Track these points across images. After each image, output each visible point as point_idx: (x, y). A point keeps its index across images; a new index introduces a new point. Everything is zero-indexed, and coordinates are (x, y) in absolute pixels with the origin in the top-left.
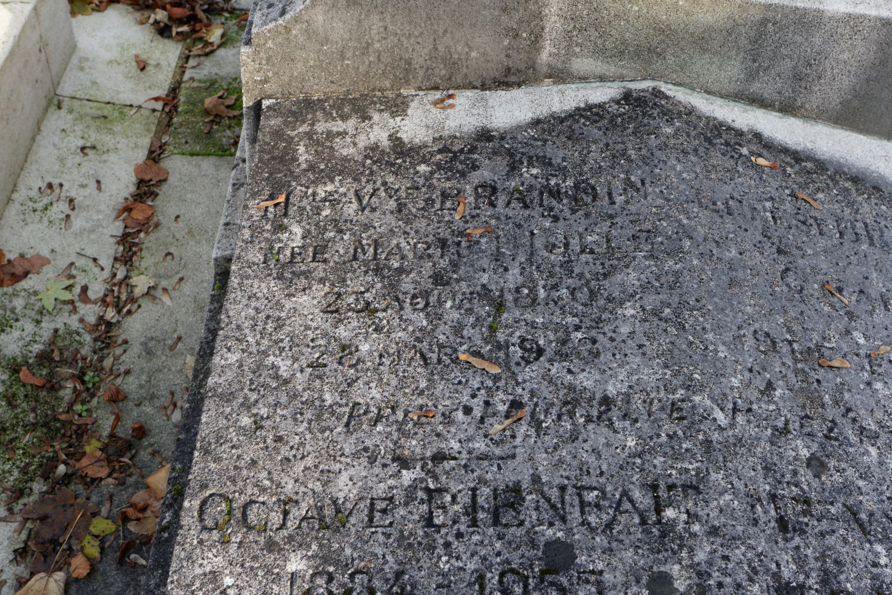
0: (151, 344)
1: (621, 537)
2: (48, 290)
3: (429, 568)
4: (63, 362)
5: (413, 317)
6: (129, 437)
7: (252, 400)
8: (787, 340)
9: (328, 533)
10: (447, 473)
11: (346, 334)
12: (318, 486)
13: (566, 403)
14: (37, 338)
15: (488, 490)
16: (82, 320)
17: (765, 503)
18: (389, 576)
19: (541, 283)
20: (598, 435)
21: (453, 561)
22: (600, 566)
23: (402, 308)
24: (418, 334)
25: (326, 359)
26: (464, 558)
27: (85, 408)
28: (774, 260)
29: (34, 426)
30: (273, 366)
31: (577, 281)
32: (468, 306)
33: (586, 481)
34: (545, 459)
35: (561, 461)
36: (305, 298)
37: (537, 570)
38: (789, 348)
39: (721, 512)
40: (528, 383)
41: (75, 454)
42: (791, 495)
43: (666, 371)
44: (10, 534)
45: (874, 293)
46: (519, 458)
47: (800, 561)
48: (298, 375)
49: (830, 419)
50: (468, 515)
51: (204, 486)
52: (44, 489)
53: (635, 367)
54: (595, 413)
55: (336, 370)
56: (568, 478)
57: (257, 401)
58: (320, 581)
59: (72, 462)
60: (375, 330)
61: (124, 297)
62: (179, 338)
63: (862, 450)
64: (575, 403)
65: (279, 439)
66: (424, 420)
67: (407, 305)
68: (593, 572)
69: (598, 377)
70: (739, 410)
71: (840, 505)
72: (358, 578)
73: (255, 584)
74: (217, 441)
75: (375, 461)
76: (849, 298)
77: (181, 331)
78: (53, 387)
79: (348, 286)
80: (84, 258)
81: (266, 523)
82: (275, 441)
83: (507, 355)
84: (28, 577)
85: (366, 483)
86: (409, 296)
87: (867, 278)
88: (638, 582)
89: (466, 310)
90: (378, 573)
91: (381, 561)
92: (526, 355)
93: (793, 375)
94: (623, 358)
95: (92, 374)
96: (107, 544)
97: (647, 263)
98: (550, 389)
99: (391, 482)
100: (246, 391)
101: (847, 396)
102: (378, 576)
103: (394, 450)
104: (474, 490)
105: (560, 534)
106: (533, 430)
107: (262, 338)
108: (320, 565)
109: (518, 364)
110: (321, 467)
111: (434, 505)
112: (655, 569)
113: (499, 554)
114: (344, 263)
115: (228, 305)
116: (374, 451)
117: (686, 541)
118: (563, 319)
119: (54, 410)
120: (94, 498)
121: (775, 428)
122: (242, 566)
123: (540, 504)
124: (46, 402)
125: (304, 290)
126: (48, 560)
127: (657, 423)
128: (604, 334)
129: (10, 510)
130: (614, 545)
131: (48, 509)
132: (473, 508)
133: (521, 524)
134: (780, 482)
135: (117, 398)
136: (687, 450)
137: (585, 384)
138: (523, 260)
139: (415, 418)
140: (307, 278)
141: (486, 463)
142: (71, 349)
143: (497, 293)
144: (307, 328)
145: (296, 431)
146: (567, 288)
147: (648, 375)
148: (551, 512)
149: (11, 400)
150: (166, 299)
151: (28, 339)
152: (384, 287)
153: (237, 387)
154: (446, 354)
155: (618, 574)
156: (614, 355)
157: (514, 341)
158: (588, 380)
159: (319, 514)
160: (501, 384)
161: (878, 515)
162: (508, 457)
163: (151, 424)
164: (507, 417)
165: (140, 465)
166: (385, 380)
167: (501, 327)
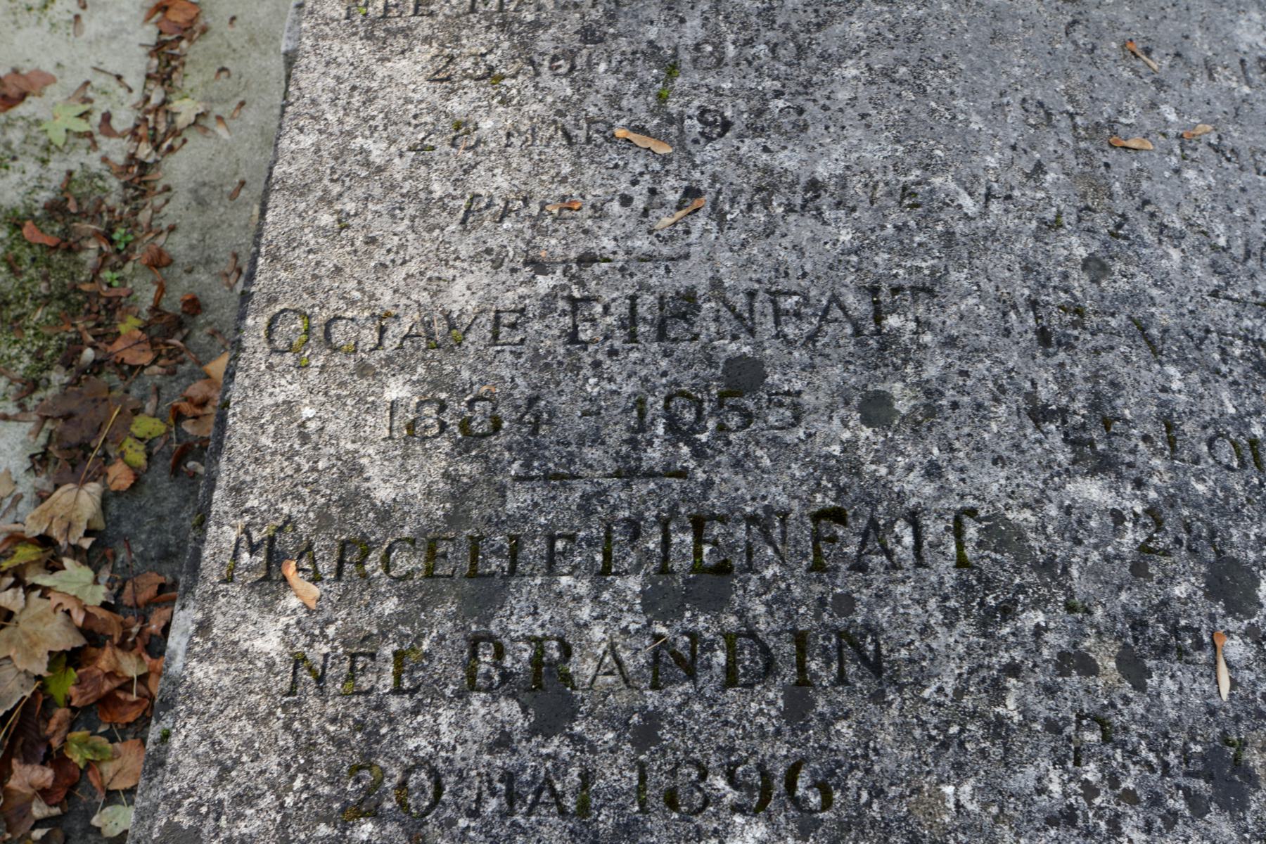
1: (827, 351)
2: (55, 118)
3: (572, 392)
4: (82, 215)
5: (553, 84)
6: (179, 313)
7: (335, 193)
8: (1067, 112)
9: (438, 354)
10: (598, 278)
11: (461, 108)
12: (425, 298)
13: (759, 190)
14: (45, 184)
15: (652, 298)
16: (105, 160)
17: (1021, 310)
18: (519, 402)
19: (731, 37)
20: (801, 228)
21: (604, 383)
22: (798, 385)
23: (538, 74)
24: (560, 106)
25: (434, 140)
26: (619, 380)
27: (116, 275)
28: (1057, 9)
29: (47, 300)
30: (362, 150)
31: (780, 33)
32: (629, 69)
33: (783, 284)
34: (728, 259)
35: (751, 261)
36: (404, 62)
37: (714, 392)
38: (1069, 121)
39: (961, 318)
40: (709, 166)
41: (105, 335)
42: (1059, 303)
43: (897, 146)
44: (24, 437)
45: (1194, 57)
46: (694, 259)
47: (1065, 381)
48: (397, 160)
49: (1120, 212)
50: (625, 329)
51: (272, 300)
52: (66, 380)
53: (855, 142)
54: (798, 201)
55: (448, 154)
56: (759, 281)
57: (341, 195)
58: (429, 410)
59: (102, 345)
60: (501, 102)
61: (162, 128)
62: (243, 183)
63: (1160, 252)
64: (772, 189)
65: (371, 241)
66: (567, 213)
67: (545, 69)
68: (788, 393)
69: (804, 156)
70: (994, 197)
71: (1124, 317)
72: (478, 406)
73: (343, 414)
74: (289, 245)
75: (501, 265)
76: (1159, 62)
77: (244, 174)
78: (70, 248)
79: (463, 46)
80: (103, 75)
81: (356, 343)
82: (367, 243)
83: (681, 131)
84: (51, 490)
85: (489, 292)
86: (548, 58)
87: (1187, 37)
88: (847, 403)
89: (626, 74)
90: (504, 399)
91: (508, 385)
92: (707, 130)
93: (1072, 156)
94: (839, 132)
95: (123, 231)
96: (156, 449)
97: (878, 8)
98: (739, 172)
99: (522, 290)
100: (326, 182)
101: (1145, 185)
102: (505, 403)
103: (526, 252)
104: (633, 298)
105: (746, 349)
106: (714, 223)
107: (346, 115)
108: (428, 391)
109: (696, 142)
110: (429, 274)
111: (579, 317)
112: (870, 388)
113: (664, 374)
114: (458, 16)
115: (299, 74)
116: (499, 254)
117: (912, 355)
118: (759, 84)
119: (73, 279)
120: (135, 392)
121: (1042, 221)
122: (326, 394)
123: (721, 313)
124: (62, 268)
125: (403, 52)
126: (77, 470)
127: (882, 212)
128: (814, 101)
129: (22, 406)
130: (818, 360)
131: (73, 405)
132: (631, 321)
133: (695, 337)
134: (1044, 286)
135: (159, 262)
136: (920, 244)
137: (786, 165)
138: (706, 8)
139: (555, 211)
140: (406, 36)
141: (650, 265)
142: (93, 198)
143: (670, 52)
144: (408, 101)
145: (392, 231)
146: (767, 43)
147: (873, 152)
148: (735, 323)
149: (13, 266)
150: (221, 131)
151: (31, 184)
152: (514, 46)
153: (313, 176)
154: (597, 131)
155: (821, 394)
156: (827, 128)
157: (690, 112)
158: (790, 159)
159: (426, 331)
160: (673, 166)
161: (1174, 332)
162: (680, 257)
163: (208, 297)
164: (679, 208)
165: (196, 349)
166: (514, 165)
167: (674, 96)
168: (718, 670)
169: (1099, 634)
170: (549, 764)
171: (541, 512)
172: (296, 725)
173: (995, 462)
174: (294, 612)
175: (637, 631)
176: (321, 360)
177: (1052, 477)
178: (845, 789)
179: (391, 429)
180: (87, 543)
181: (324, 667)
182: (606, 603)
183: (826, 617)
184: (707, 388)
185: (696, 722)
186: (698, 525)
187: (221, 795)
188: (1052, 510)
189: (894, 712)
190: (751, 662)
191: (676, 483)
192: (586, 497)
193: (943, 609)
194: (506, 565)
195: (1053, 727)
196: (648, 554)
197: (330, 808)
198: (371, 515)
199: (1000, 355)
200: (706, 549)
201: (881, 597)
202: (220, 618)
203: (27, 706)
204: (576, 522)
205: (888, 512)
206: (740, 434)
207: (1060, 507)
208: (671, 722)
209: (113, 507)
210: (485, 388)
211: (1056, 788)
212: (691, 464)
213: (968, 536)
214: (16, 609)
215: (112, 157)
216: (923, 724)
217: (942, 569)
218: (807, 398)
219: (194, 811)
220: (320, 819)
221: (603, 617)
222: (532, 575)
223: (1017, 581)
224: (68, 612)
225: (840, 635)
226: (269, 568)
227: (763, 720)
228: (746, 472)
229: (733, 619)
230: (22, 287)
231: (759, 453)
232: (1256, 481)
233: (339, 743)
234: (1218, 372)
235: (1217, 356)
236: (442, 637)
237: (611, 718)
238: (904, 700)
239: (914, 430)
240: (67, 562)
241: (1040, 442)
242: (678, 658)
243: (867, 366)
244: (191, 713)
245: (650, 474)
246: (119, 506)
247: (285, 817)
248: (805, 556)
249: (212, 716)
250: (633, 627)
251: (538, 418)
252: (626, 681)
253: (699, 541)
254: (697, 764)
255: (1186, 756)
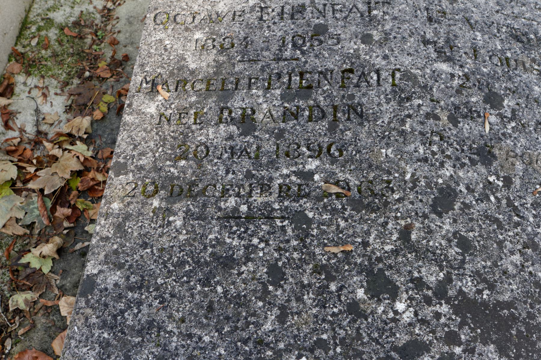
0: (131, 19)
4: (86, 26)
9: (213, 24)
12: (209, 8)
14: (72, 15)
16: (95, 8)
21: (271, 33)
22: (339, 32)
27: (98, 47)
29: (72, 55)
39: (400, 11)
41: (93, 67)
47: (436, 33)
51: (156, 9)
52: (79, 82)
59: (92, 71)
73: (179, 43)
78: (81, 38)
96: (111, 107)
99: (244, 5)
104: (283, 7)
105: (321, 22)
112: (365, 32)
113: (292, 29)
117: (381, 22)
124: (78, 44)
129: (62, 91)
130: (347, 24)
131: (81, 90)
132: (281, 14)
133: (304, 18)
134: (431, 4)
135: (114, 43)
142: (90, 21)
148: (318, 14)
151: (68, 15)
155: (347, 35)
161: (480, 22)
168: (306, 117)
169: (442, 109)
170: (246, 144)
171: (247, 71)
172: (160, 133)
173: (408, 55)
174: (161, 101)
175: (278, 106)
176: (173, 26)
177: (429, 61)
178: (347, 151)
179: (196, 47)
180: (85, 136)
181: (170, 117)
182: (268, 97)
183: (344, 101)
184: (307, 33)
185: (297, 132)
186: (301, 75)
187: (134, 153)
188: (428, 71)
189: (366, 128)
190: (318, 114)
191: (294, 62)
192: (263, 67)
193: (385, 98)
194: (234, 87)
195: (421, 133)
196: (284, 83)
197: (170, 157)
198: (188, 72)
199: (413, 23)
200: (304, 81)
201: (364, 95)
202: (135, 103)
203: (62, 188)
204: (259, 74)
205: (369, 69)
206: (318, 47)
207: (431, 70)
208: (289, 132)
209: (95, 125)
210: (229, 34)
211: (421, 151)
212: (300, 56)
213: (396, 77)
214: (59, 156)
215: (97, 7)
216: (376, 132)
217: (386, 86)
218: (343, 36)
219: (125, 158)
220: (167, 160)
221: (267, 101)
222: (243, 90)
223: (413, 90)
224: (78, 157)
225: (349, 106)
226: (152, 89)
227: (321, 131)
228: (319, 58)
229: (312, 102)
230: (63, 50)
231: (324, 52)
232: (506, 70)
233: (174, 138)
234: (496, 36)
235: (496, 31)
236: (211, 108)
237: (268, 131)
238: (370, 125)
239: (380, 45)
240: (78, 142)
241: (426, 50)
242: (292, 114)
243: (364, 26)
244: (124, 130)
245: (286, 60)
246: (97, 126)
247: (156, 159)
248: (338, 83)
249: (132, 131)
250: (277, 105)
251: (247, 43)
252: (274, 121)
253: (302, 79)
254: (297, 144)
255: (471, 148)
